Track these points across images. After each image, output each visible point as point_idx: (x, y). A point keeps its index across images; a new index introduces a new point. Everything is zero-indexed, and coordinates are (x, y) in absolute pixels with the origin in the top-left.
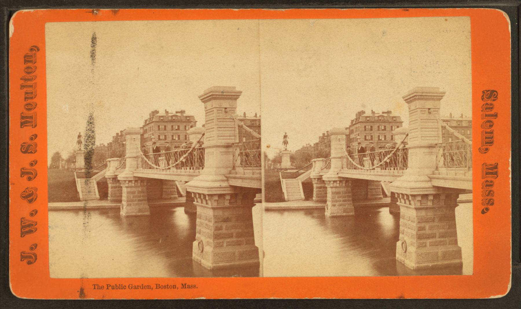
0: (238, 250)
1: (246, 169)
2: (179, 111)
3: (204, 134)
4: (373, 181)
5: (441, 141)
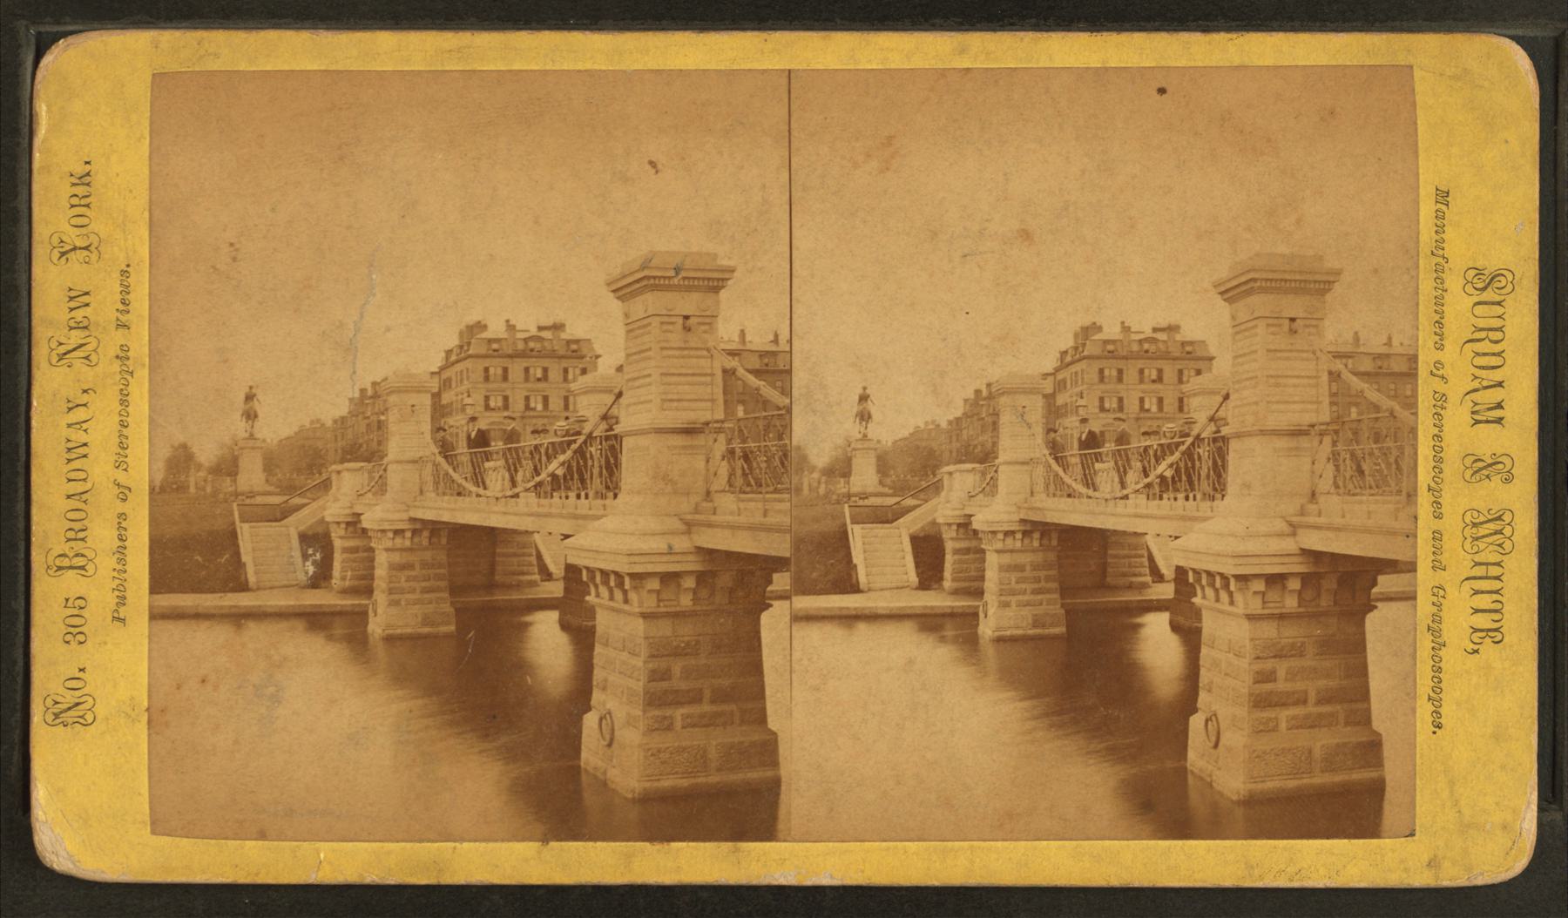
0: (715, 741)
2: (1164, 324)
3: (620, 395)
5: (720, 415)
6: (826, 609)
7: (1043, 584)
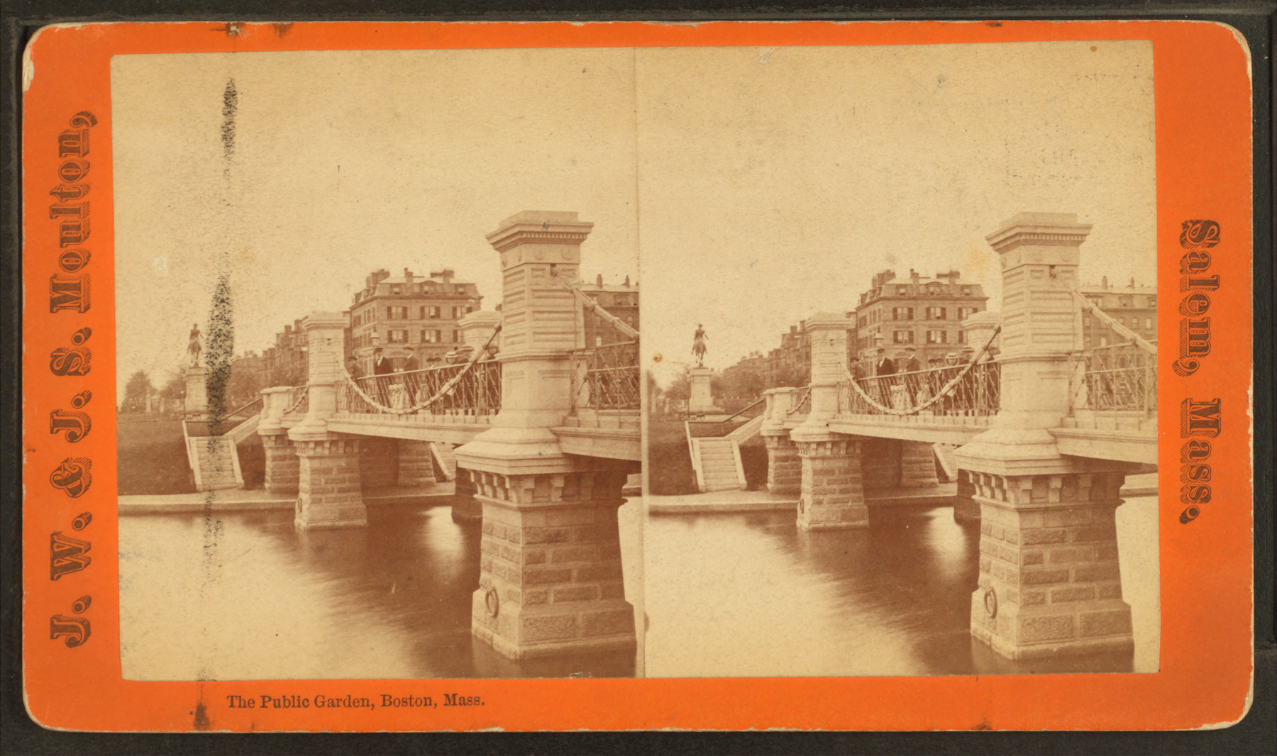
0: (583, 612)
1: (602, 414)
2: (440, 270)
3: (499, 329)
4: (915, 443)
6: (176, 506)
7: (849, 485)
